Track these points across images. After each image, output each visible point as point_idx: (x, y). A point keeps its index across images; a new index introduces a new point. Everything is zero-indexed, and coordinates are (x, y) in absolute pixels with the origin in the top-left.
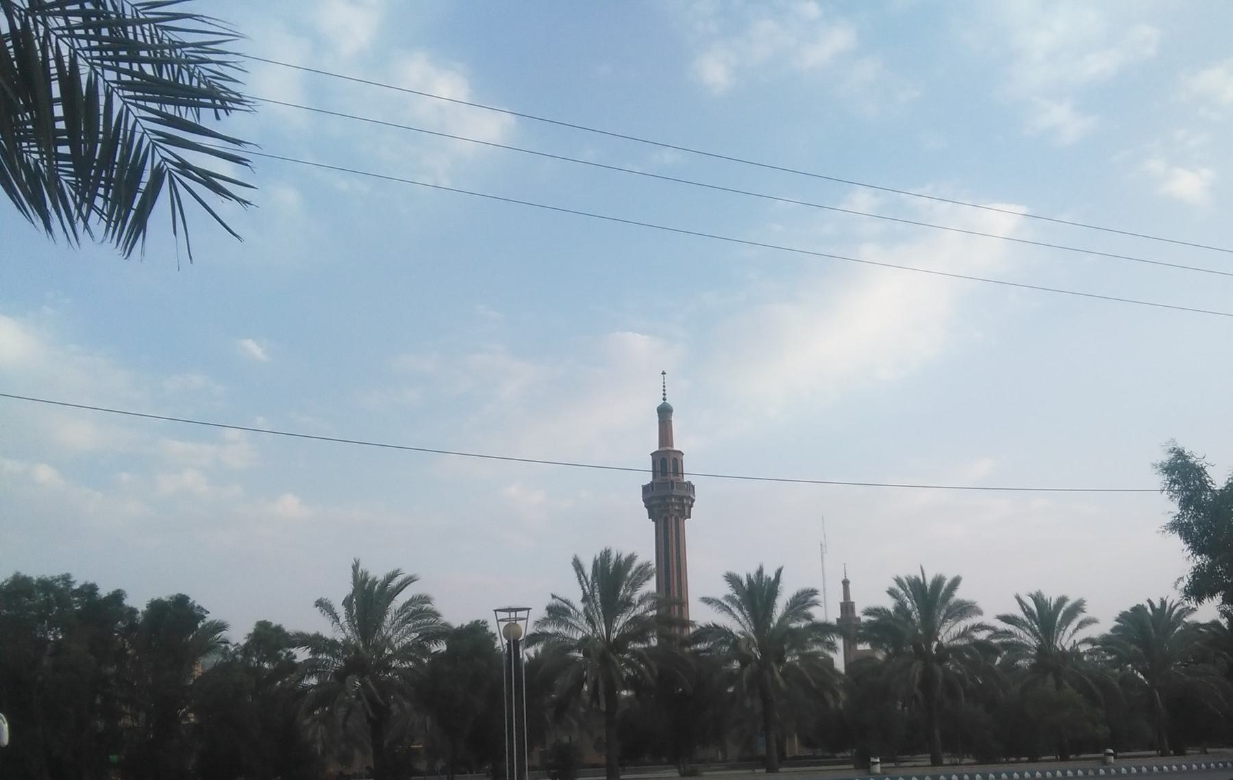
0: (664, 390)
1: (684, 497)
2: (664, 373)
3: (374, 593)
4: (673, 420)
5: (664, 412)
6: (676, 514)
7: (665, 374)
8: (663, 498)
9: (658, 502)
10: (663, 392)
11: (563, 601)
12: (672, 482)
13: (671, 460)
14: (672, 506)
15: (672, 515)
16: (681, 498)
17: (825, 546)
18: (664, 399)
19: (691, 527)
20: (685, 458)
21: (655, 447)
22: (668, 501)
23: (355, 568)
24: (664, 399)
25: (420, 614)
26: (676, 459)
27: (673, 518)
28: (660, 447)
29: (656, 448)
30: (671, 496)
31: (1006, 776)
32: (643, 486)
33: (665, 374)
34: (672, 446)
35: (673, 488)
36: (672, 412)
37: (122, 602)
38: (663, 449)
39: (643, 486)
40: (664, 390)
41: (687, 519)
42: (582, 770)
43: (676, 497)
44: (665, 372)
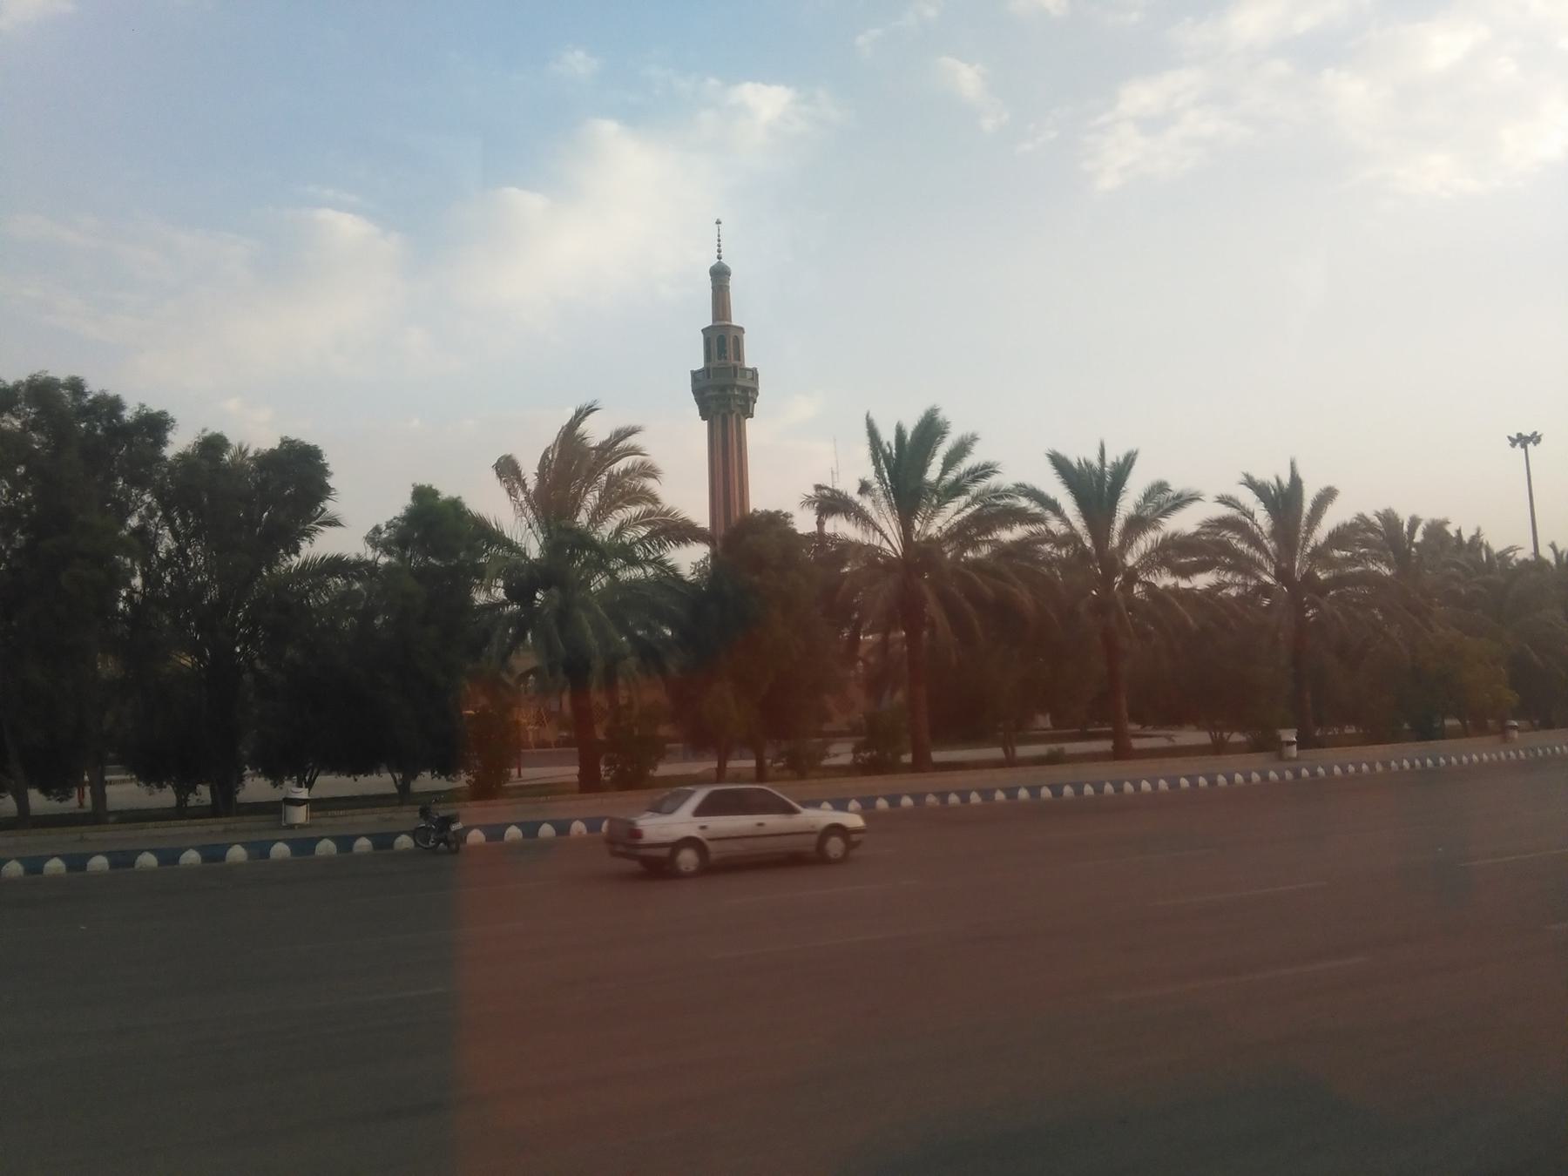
0: (719, 246)
1: (749, 388)
2: (718, 222)
3: (906, 443)
4: (730, 284)
5: (720, 275)
6: (738, 410)
7: (720, 223)
8: (723, 389)
9: (716, 393)
10: (717, 248)
11: (978, 477)
12: (735, 367)
13: (732, 340)
14: (734, 399)
15: (733, 412)
16: (745, 390)
17: (838, 473)
18: (719, 258)
19: (755, 431)
20: (745, 336)
21: (708, 321)
22: (729, 392)
23: (868, 416)
24: (719, 258)
25: (633, 496)
26: (736, 337)
27: (734, 415)
28: (713, 321)
29: (709, 323)
30: (734, 386)
31: (1276, 776)
32: (692, 372)
33: (720, 223)
34: (730, 321)
35: (735, 375)
36: (729, 274)
37: (236, 471)
38: (718, 323)
39: (692, 372)
40: (719, 246)
41: (749, 419)
42: (110, 767)
43: (739, 387)
44: (721, 220)
